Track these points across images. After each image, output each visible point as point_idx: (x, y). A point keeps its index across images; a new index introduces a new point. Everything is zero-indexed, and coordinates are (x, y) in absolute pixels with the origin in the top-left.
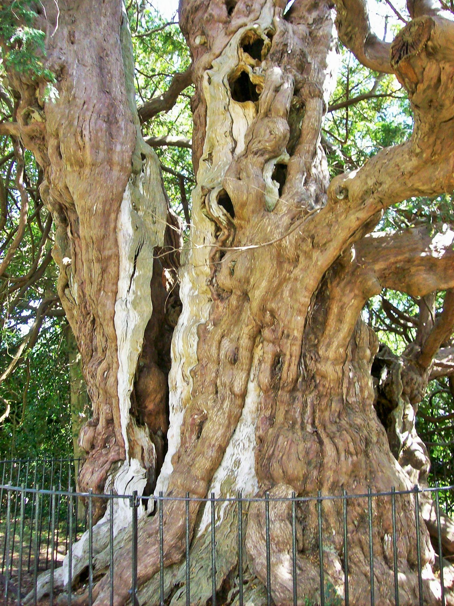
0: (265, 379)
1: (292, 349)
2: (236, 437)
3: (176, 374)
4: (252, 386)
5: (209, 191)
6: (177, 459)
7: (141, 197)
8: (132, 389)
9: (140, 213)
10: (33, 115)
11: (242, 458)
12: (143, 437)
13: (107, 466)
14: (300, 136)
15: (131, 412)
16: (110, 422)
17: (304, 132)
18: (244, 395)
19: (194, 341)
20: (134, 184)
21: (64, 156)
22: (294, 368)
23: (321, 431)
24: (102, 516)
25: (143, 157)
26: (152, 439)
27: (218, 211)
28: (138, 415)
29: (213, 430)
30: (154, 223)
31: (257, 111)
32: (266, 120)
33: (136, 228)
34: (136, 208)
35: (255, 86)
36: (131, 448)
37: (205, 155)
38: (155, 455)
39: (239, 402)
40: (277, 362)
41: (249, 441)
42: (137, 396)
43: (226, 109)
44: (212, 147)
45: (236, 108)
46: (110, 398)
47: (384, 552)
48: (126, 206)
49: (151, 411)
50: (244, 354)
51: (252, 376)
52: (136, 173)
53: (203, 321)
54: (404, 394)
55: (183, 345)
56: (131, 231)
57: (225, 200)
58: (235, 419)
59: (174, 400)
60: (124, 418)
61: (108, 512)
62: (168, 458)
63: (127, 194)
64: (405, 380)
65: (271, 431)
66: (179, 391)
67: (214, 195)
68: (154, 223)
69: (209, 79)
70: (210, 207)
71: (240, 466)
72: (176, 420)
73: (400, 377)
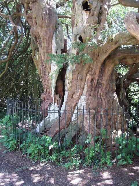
0: (89, 84)
1: (96, 77)
2: (81, 98)
3: (67, 82)
4: (85, 86)
5: (77, 36)
6: (67, 103)
7: (58, 35)
8: (55, 85)
9: (58, 40)
10: (28, 12)
11: (83, 103)
12: (57, 97)
13: (48, 104)
14: (101, 21)
15: (55, 91)
16: (49, 93)
17: (102, 20)
18: (84, 88)
19: (71, 74)
20: (56, 32)
21: (38, 24)
22: (96, 82)
23: (102, 97)
24: (47, 116)
25: (58, 24)
26: (60, 98)
27: (78, 41)
28: (56, 92)
29: (76, 97)
30: (61, 42)
31: (90, 14)
32: (92, 17)
33: (57, 44)
34: (56, 38)
35: (89, 6)
36: (55, 100)
37: (75, 25)
38: (60, 102)
39: (82, 89)
40: (92, 81)
41: (85, 99)
42: (56, 88)
43: (81, 13)
44: (77, 23)
45: (84, 13)
46: (49, 87)
47: (115, 127)
48: (54, 38)
49: (60, 90)
50: (84, 78)
51: (86, 84)
52: (56, 29)
53: (74, 69)
54: (123, 87)
55: (68, 75)
56: (55, 45)
57: (80, 38)
58: (81, 94)
59: (66, 88)
60: (53, 93)
61: (48, 115)
62: (64, 103)
63: (54, 35)
64: (124, 83)
65: (90, 97)
66: (67, 86)
67: (78, 37)
68: (61, 42)
69: (77, 3)
70: (77, 40)
71: (82, 103)
72: (66, 93)
73: (123, 82)
